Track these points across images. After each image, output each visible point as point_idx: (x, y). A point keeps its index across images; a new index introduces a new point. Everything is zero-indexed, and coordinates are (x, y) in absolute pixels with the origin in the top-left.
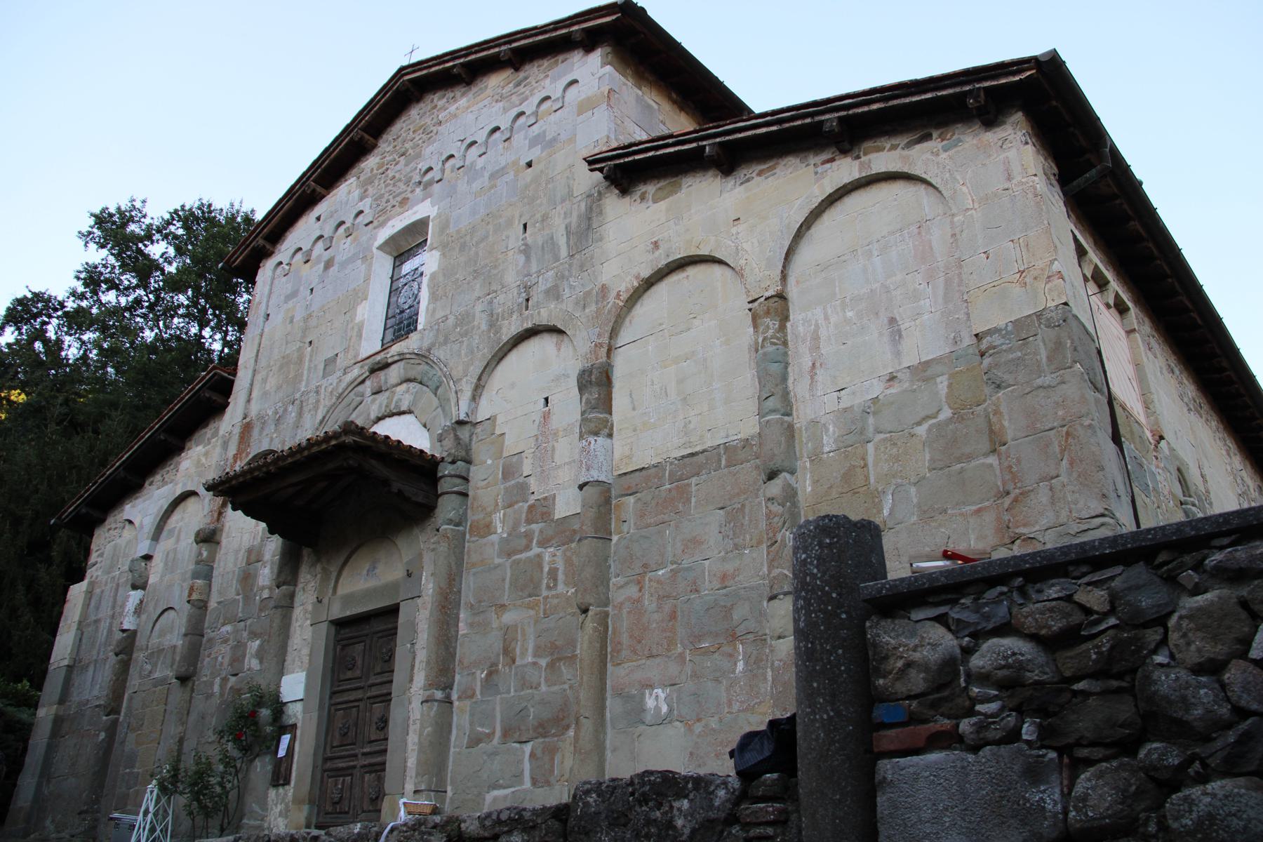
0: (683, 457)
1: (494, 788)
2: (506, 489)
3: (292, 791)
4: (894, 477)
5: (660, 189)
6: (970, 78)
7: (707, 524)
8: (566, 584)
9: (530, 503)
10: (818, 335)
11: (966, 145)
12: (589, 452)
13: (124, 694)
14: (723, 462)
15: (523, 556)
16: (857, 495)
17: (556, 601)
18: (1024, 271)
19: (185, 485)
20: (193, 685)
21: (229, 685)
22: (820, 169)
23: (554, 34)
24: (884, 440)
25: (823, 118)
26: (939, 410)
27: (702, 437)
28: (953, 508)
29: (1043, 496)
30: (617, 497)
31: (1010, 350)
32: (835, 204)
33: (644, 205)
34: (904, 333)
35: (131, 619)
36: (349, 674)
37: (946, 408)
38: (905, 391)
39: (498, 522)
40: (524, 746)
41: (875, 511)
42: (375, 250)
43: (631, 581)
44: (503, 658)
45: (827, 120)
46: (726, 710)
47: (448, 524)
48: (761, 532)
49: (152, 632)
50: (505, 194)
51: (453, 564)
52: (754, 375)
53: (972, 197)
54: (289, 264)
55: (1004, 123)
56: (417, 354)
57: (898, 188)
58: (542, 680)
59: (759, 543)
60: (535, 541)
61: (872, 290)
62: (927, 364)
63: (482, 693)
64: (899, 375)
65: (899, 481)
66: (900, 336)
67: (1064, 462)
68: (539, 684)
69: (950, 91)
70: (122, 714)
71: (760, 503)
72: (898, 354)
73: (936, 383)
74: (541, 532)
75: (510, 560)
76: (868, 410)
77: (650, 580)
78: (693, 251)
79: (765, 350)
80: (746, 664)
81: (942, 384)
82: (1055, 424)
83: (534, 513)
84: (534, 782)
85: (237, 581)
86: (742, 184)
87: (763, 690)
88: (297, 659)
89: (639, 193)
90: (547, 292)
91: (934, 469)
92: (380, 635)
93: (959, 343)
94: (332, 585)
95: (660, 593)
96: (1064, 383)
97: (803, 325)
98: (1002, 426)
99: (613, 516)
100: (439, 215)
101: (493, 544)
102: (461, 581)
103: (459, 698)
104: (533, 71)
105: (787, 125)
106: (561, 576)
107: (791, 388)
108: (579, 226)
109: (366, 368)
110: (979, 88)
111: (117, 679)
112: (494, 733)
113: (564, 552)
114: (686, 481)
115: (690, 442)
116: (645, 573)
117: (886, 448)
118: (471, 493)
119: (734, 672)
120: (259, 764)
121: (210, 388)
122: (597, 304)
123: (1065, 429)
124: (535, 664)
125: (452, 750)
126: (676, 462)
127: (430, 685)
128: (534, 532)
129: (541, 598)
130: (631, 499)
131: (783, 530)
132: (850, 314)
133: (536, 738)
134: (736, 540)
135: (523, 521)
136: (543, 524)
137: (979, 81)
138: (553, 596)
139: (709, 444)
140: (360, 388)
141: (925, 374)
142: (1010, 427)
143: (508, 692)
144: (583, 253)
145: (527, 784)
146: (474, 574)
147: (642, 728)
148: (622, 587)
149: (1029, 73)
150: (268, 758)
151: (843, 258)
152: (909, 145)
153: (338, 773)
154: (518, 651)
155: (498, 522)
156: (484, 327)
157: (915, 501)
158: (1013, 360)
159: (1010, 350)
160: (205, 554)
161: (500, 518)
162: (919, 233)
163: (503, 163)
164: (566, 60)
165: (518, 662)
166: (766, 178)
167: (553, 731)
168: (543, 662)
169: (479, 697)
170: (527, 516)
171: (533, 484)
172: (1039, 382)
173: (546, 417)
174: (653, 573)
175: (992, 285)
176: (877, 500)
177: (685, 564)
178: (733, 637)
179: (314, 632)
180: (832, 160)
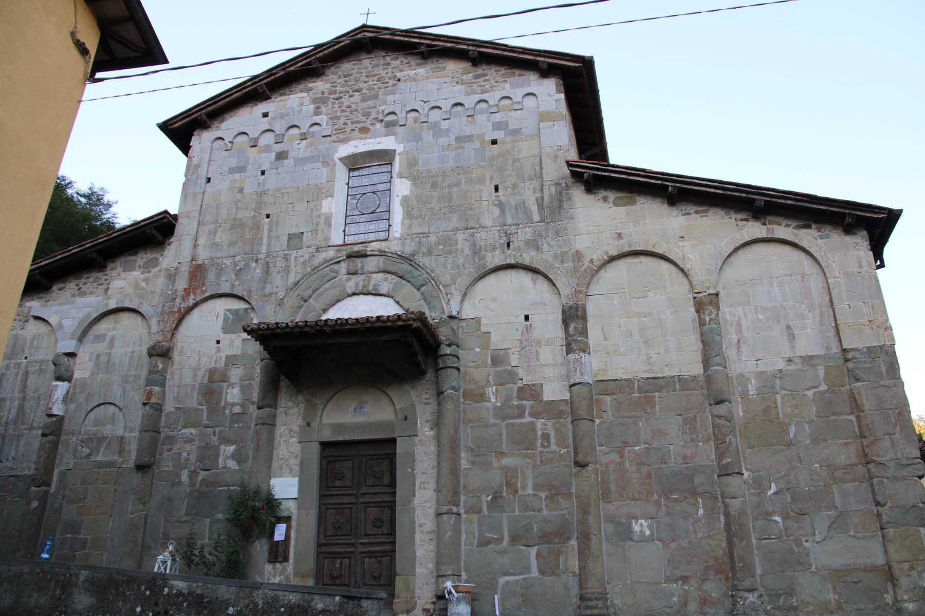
0: (648, 378)
1: (504, 575)
2: (496, 373)
3: (291, 566)
4: (795, 417)
7: (669, 423)
8: (558, 445)
9: (518, 385)
10: (740, 324)
12: (581, 363)
13: (53, 469)
15: (518, 421)
18: (871, 321)
19: (118, 301)
20: (154, 472)
21: (200, 478)
23: (521, 56)
24: (788, 394)
27: (661, 369)
28: (831, 440)
29: (887, 443)
31: (864, 362)
33: (606, 205)
35: (60, 406)
36: (338, 483)
37: (823, 384)
38: (798, 370)
39: (491, 394)
40: (529, 549)
42: (337, 160)
43: (613, 451)
44: (507, 489)
45: (758, 199)
46: (693, 536)
47: (452, 390)
49: (84, 420)
50: (473, 156)
52: (697, 338)
54: (231, 142)
55: (854, 234)
56: (398, 255)
57: (787, 250)
58: (544, 506)
59: (709, 440)
60: (527, 413)
61: (774, 306)
62: (811, 357)
63: (488, 510)
64: (794, 359)
65: (798, 419)
66: (794, 338)
67: (898, 427)
68: (541, 509)
69: (837, 210)
70: (54, 486)
71: (707, 417)
72: (793, 347)
74: (532, 407)
77: (629, 452)
80: (705, 510)
81: (821, 371)
82: (892, 407)
83: (524, 393)
84: (542, 572)
85: (199, 394)
86: (683, 215)
87: (718, 527)
88: (284, 466)
90: (528, 242)
92: (368, 457)
94: (320, 414)
95: (638, 461)
96: (896, 386)
97: (730, 315)
100: (405, 153)
101: (488, 409)
103: (466, 512)
104: (493, 73)
106: (553, 440)
107: (725, 352)
108: (551, 203)
109: (345, 253)
111: (49, 457)
112: (502, 538)
115: (652, 370)
119: (697, 514)
120: (258, 545)
121: (156, 228)
122: (574, 262)
123: (898, 410)
124: (535, 495)
125: (463, 548)
126: (642, 380)
127: (448, 502)
130: (608, 398)
131: (730, 436)
132: (761, 317)
133: (542, 544)
134: (692, 436)
135: (515, 397)
137: (855, 210)
138: (548, 452)
139: (667, 374)
140: (336, 267)
142: (867, 403)
143: (514, 511)
144: (558, 223)
145: (535, 572)
147: (630, 543)
148: (606, 453)
149: (883, 216)
150: (264, 541)
151: (754, 281)
152: (798, 227)
153: (334, 556)
154: (519, 485)
155: (491, 394)
158: (866, 368)
159: (864, 362)
160: (161, 366)
161: (493, 392)
162: (803, 281)
163: (468, 133)
164: (523, 75)
165: (520, 492)
166: (701, 217)
167: (556, 541)
168: (543, 495)
169: (486, 513)
170: (517, 394)
171: (521, 373)
172: (883, 383)
177: (655, 445)
178: (694, 493)
179: (302, 449)
180: (747, 220)
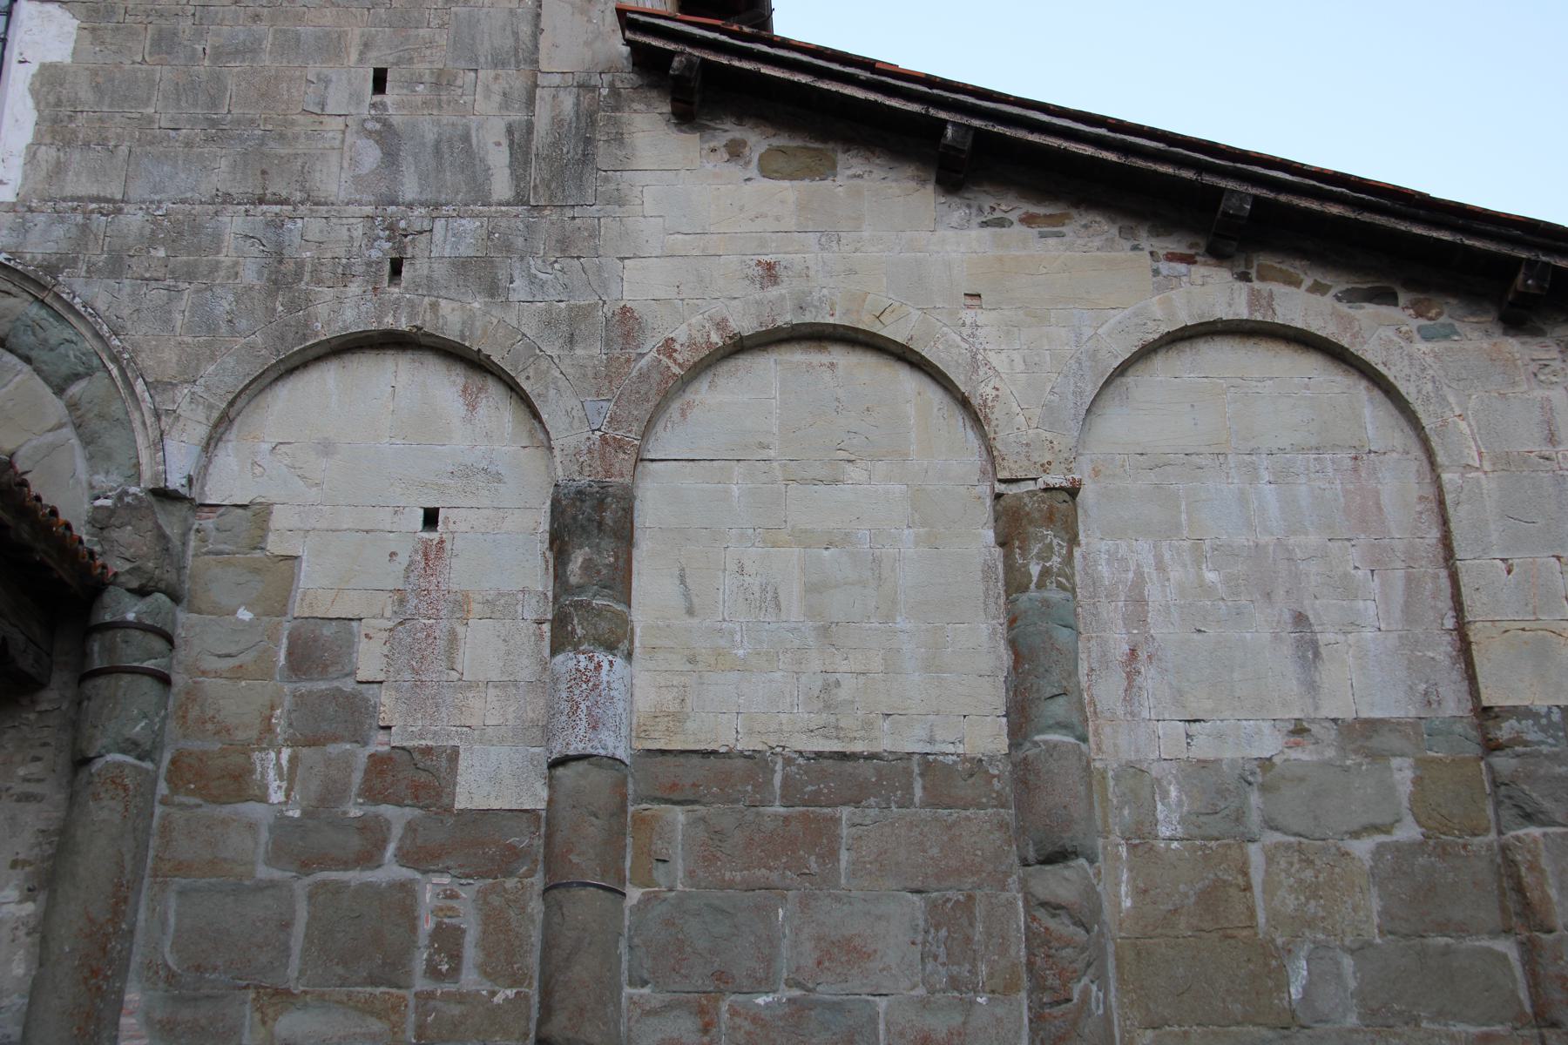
2: (301, 700)
5: (781, 150)
6: (1529, 238)
7: (879, 918)
8: (486, 971)
9: (371, 749)
10: (1141, 593)
11: (1469, 345)
12: (596, 686)
14: (918, 793)
15: (354, 876)
16: (1232, 942)
17: (456, 1010)
22: (1165, 267)
25: (1223, 183)
26: (1397, 821)
27: (867, 725)
28: (1432, 1020)
30: (640, 799)
32: (1180, 346)
33: (735, 170)
34: (1323, 650)
39: (272, 774)
41: (1271, 984)
47: (124, 751)
48: (1014, 965)
51: (128, 857)
53: (1478, 446)
57: (1310, 366)
60: (391, 848)
64: (1315, 728)
65: (1321, 936)
66: (1317, 654)
69: (1491, 246)
71: (1011, 904)
72: (1312, 687)
73: (1389, 768)
74: (411, 827)
75: (307, 880)
76: (1251, 779)
77: (734, 1012)
78: (866, 323)
79: (1046, 594)
81: (1402, 774)
83: (389, 779)
86: (985, 224)
89: (723, 139)
91: (1391, 933)
93: (1434, 706)
98: (1546, 898)
99: (629, 840)
101: (252, 827)
102: (137, 903)
105: (1141, 163)
106: (471, 953)
110: (1547, 264)
113: (484, 894)
114: (826, 810)
115: (837, 728)
116: (722, 992)
117: (1291, 864)
118: (179, 679)
122: (608, 343)
126: (801, 761)
128: (388, 823)
129: (409, 995)
130: (679, 815)
131: (1085, 980)
132: (1211, 576)
135: (355, 789)
136: (417, 812)
137: (1549, 250)
138: (447, 996)
141: (1368, 744)
144: (569, 213)
146: (182, 893)
148: (653, 1012)
152: (1351, 297)
155: (272, 774)
156: (249, 274)
157: (1352, 984)
162: (1355, 470)
166: (1043, 236)
170: (366, 780)
171: (388, 704)
173: (432, 556)
174: (741, 998)
175: (1522, 625)
176: (1274, 963)
180: (1189, 260)
